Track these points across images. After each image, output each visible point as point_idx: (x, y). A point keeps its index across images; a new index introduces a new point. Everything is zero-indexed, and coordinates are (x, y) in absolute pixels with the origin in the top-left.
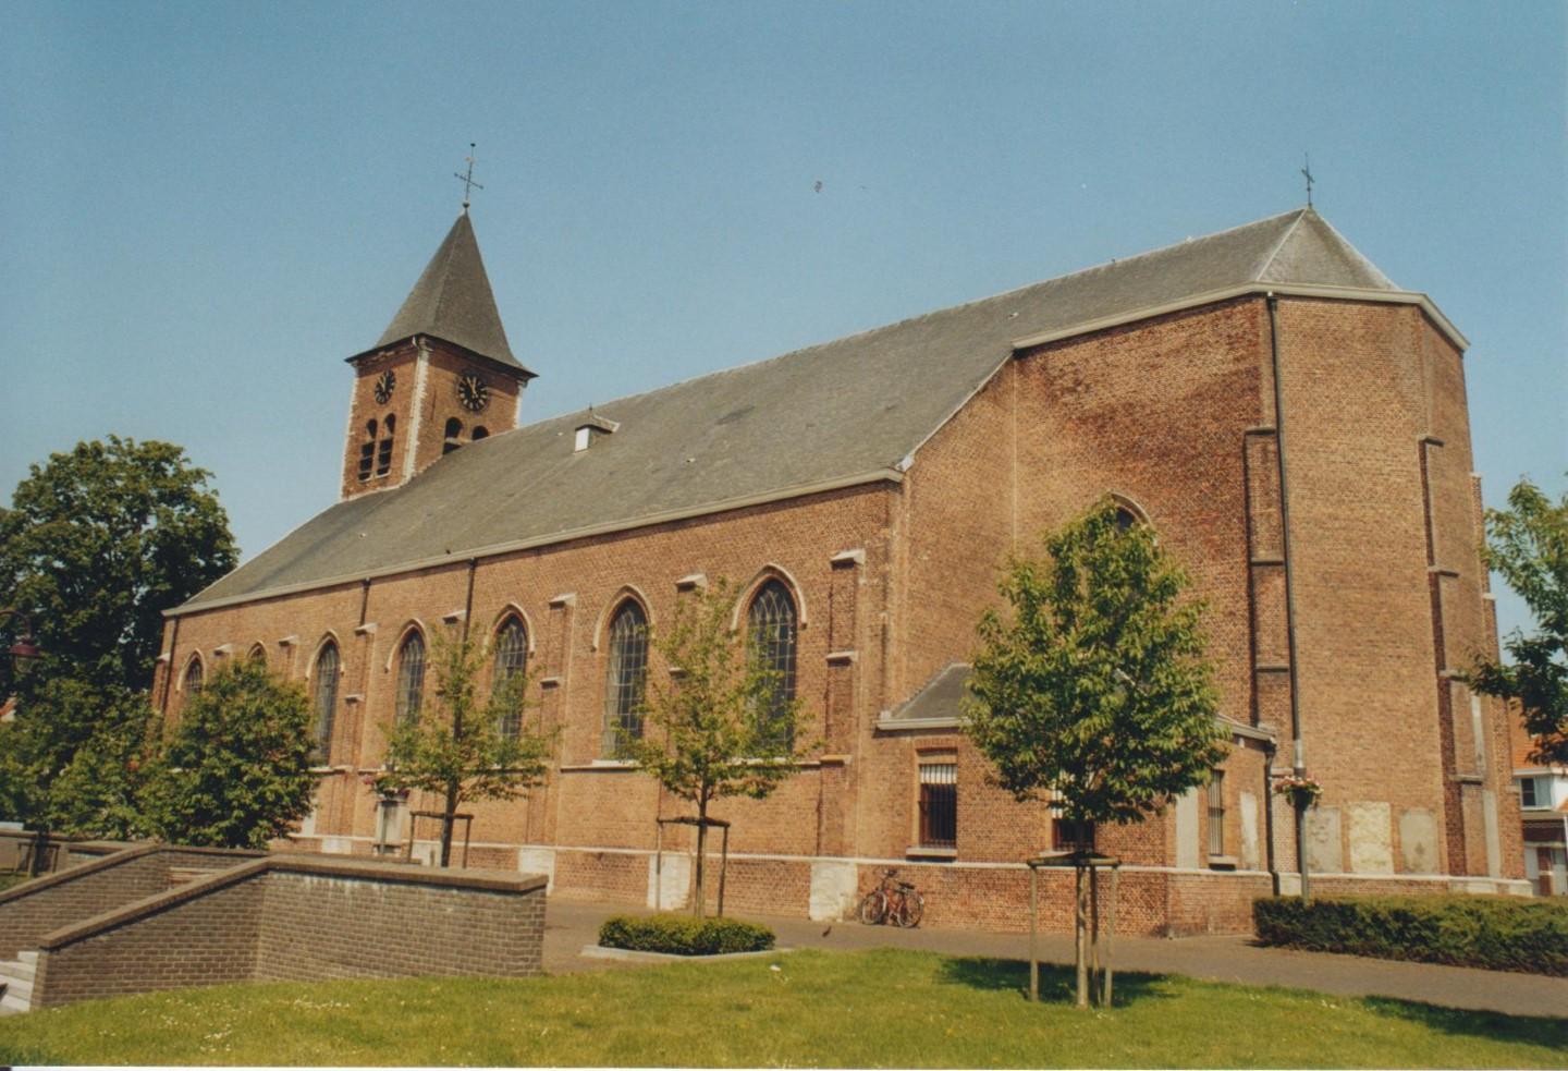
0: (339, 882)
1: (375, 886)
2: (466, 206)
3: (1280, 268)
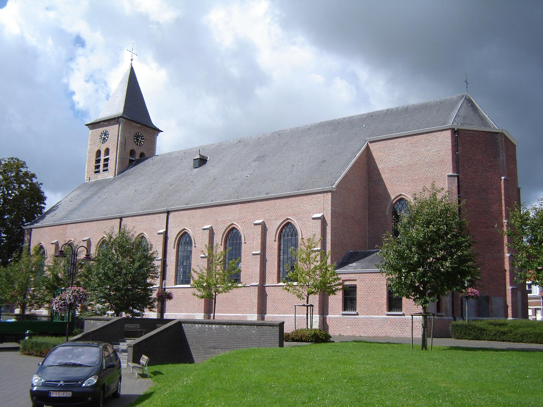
0: (210, 326)
1: (225, 326)
2: (132, 60)
3: (459, 119)
